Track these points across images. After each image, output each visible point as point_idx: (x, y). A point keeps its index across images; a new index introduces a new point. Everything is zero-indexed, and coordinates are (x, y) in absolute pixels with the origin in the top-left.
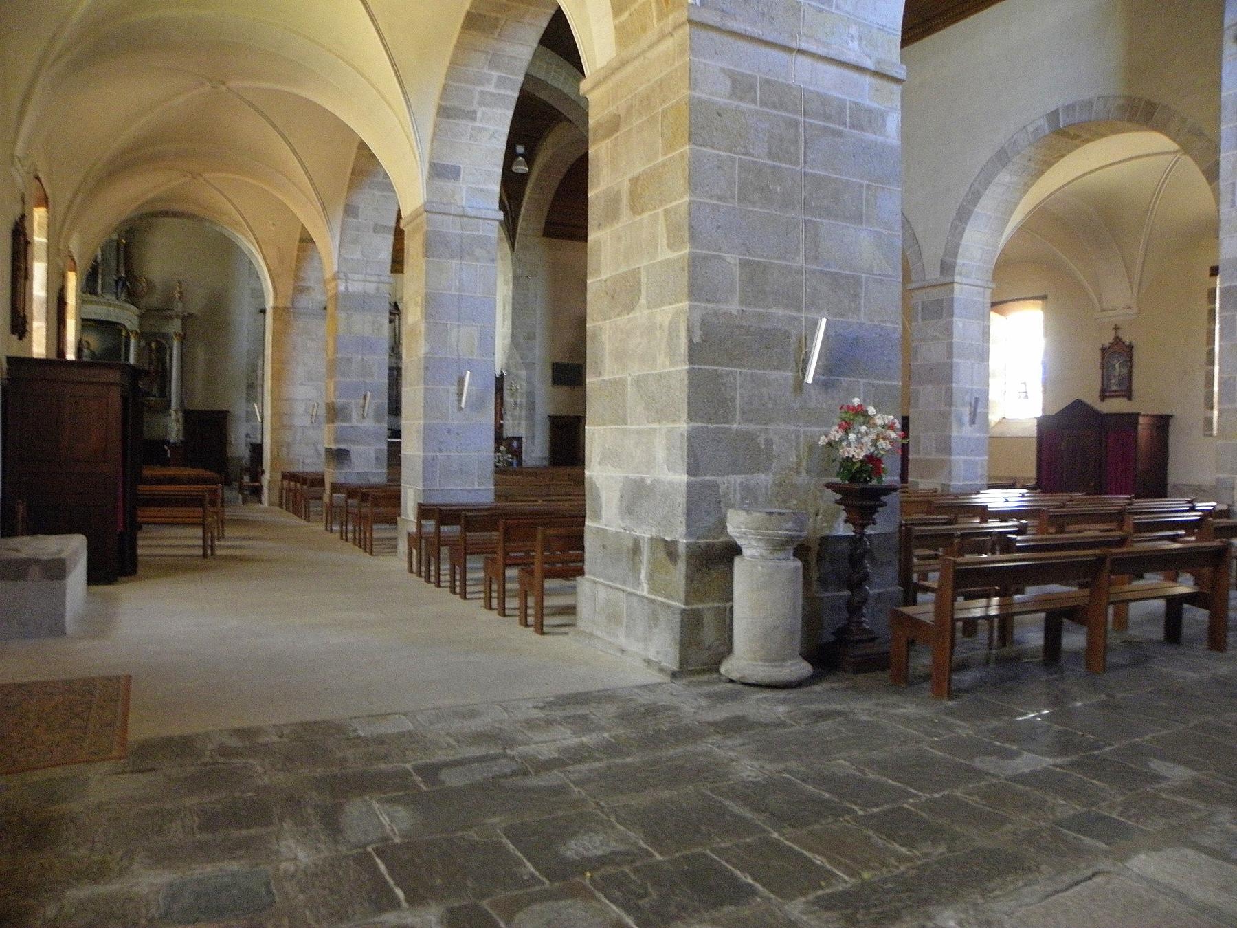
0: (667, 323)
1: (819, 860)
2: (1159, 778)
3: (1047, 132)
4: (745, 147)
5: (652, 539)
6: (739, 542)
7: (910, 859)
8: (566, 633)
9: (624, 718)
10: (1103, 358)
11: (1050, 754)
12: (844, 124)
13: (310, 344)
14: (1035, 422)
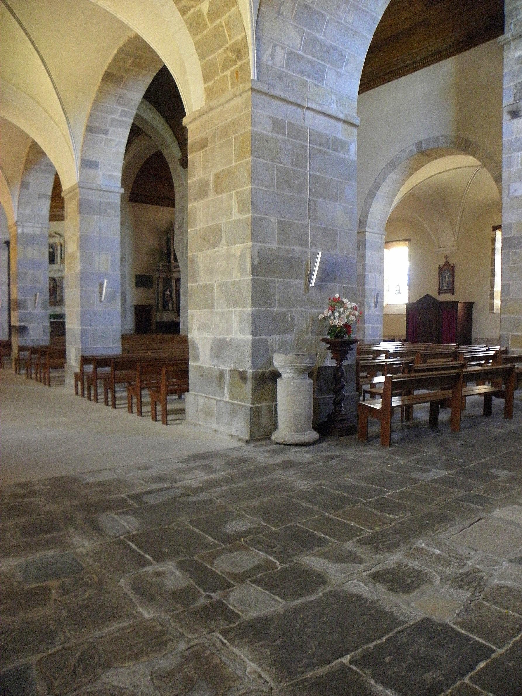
0: (239, 254)
1: (352, 524)
2: (496, 477)
3: (416, 152)
4: (280, 159)
5: (231, 370)
6: (280, 371)
7: (396, 520)
8: (180, 424)
9: (229, 464)
10: (439, 272)
11: (445, 470)
12: (329, 148)
14: (405, 306)
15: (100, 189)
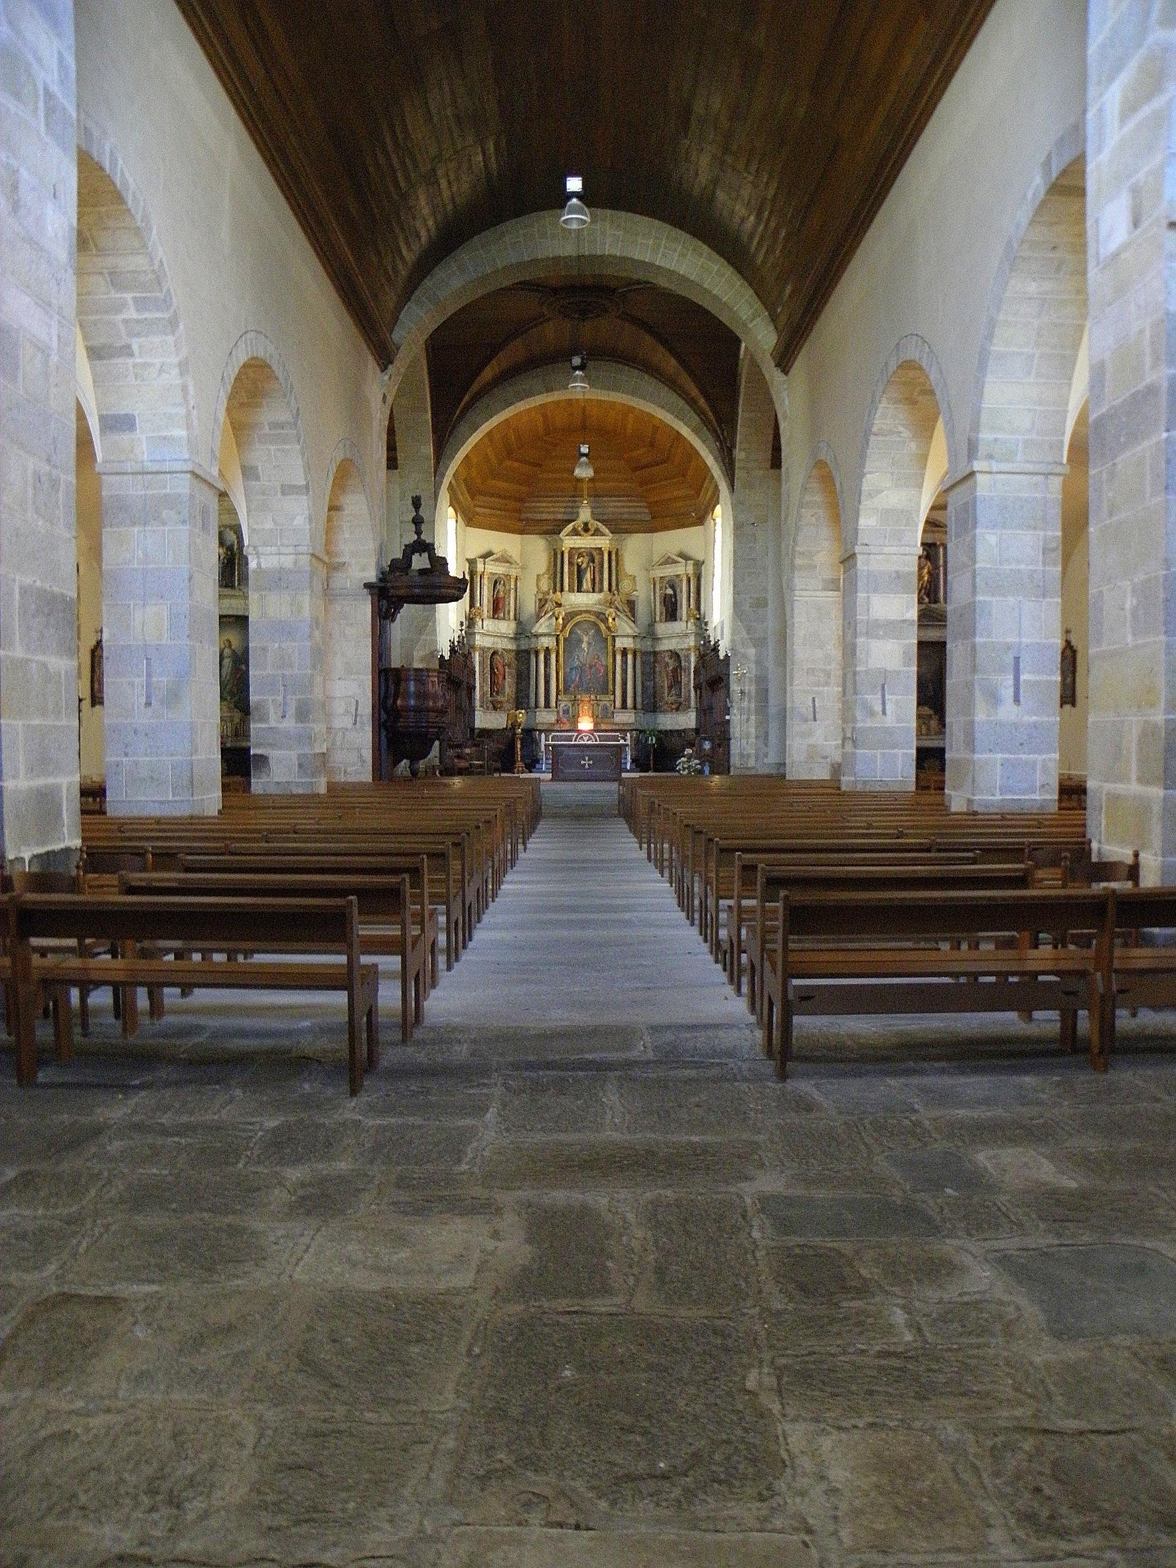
13: (350, 631)
15: (141, 470)
